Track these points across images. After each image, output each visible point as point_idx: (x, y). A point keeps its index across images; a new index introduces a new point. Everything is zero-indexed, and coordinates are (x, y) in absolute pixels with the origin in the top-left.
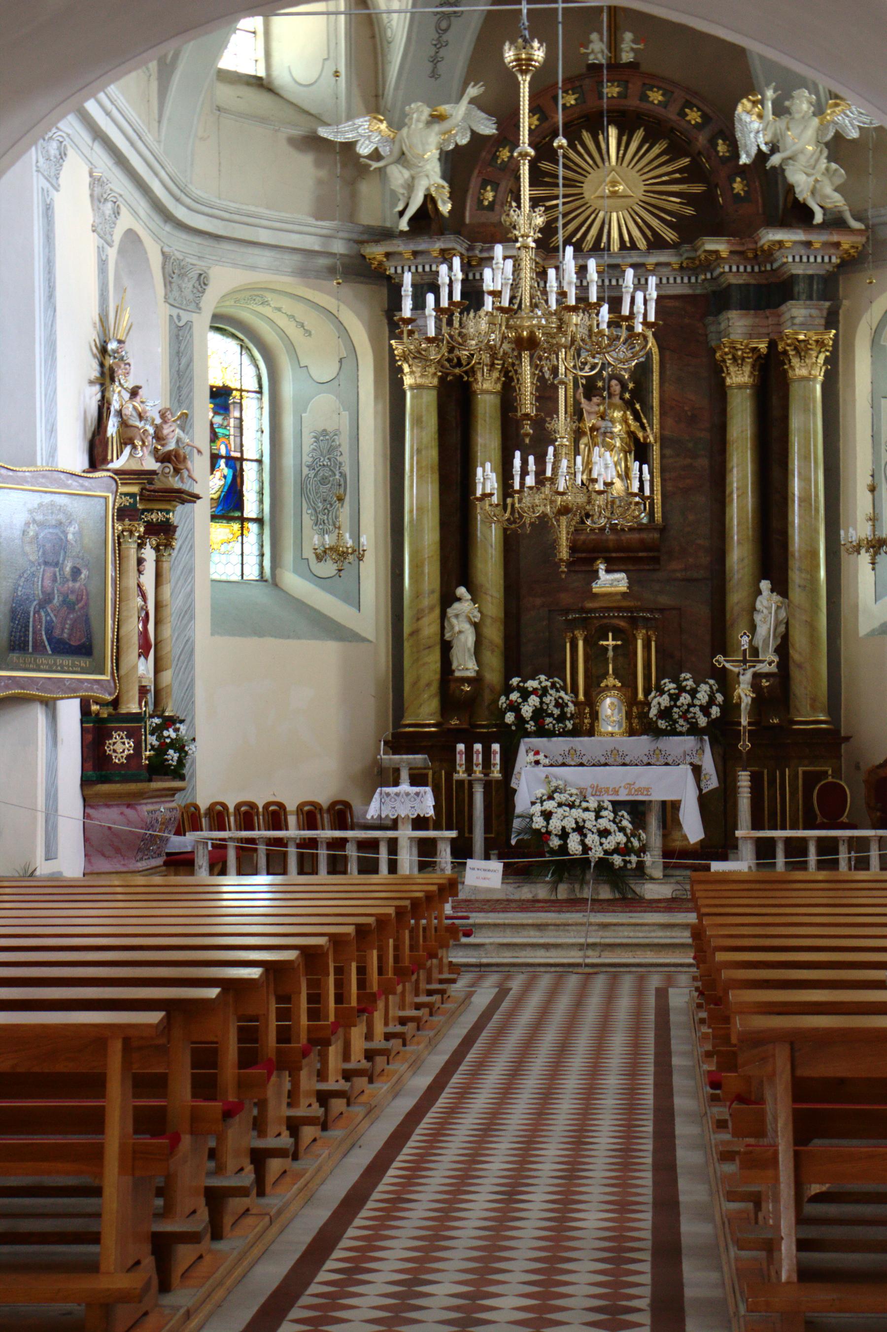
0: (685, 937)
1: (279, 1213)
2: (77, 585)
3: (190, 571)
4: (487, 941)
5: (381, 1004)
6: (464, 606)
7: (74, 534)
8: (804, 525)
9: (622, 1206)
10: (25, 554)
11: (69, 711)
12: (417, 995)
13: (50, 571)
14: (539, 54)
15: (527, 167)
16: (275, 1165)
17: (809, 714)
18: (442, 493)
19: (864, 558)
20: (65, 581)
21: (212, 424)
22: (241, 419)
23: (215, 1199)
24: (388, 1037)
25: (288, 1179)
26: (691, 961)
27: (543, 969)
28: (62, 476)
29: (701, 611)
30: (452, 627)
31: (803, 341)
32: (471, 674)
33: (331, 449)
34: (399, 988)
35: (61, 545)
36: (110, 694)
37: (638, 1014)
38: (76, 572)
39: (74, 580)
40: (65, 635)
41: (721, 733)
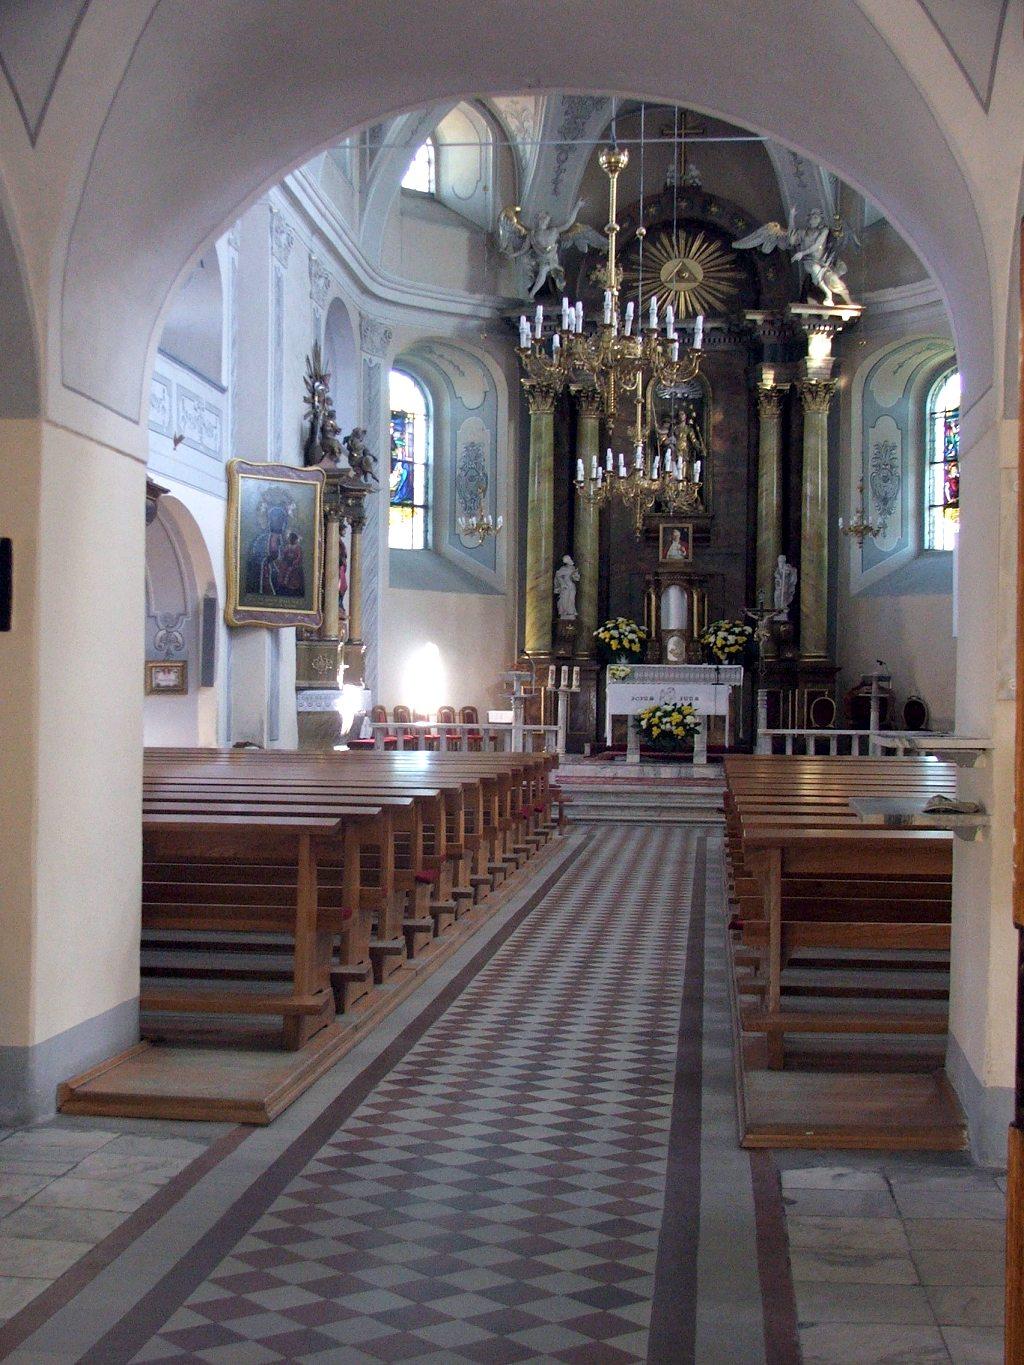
0: (720, 803)
1: (423, 968)
2: (295, 546)
3: (375, 541)
4: (581, 803)
5: (500, 835)
6: (568, 571)
7: (293, 510)
8: (813, 517)
9: (664, 973)
10: (258, 524)
11: (288, 635)
12: (527, 834)
13: (275, 536)
14: (624, 159)
15: (614, 238)
16: (421, 938)
17: (812, 651)
18: (556, 488)
19: (854, 540)
20: (285, 542)
21: (392, 438)
22: (412, 434)
23: (377, 956)
24: (505, 860)
25: (430, 947)
26: (724, 819)
27: (619, 824)
28: (285, 469)
29: (737, 574)
30: (560, 585)
31: (814, 385)
32: (572, 618)
33: (477, 456)
34: (514, 826)
35: (284, 518)
36: (317, 624)
37: (684, 852)
38: (294, 537)
39: (293, 543)
40: (285, 582)
41: (746, 656)
